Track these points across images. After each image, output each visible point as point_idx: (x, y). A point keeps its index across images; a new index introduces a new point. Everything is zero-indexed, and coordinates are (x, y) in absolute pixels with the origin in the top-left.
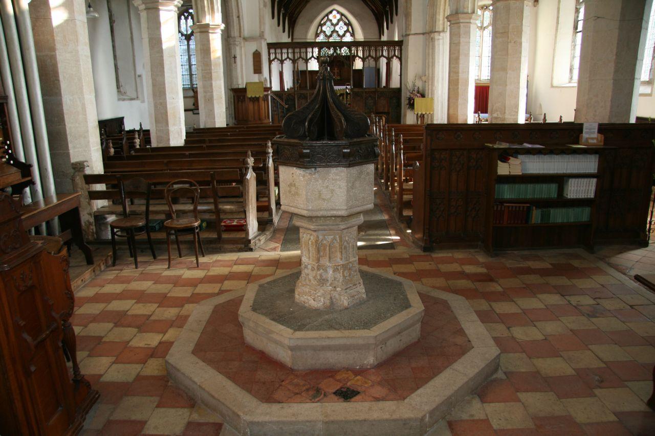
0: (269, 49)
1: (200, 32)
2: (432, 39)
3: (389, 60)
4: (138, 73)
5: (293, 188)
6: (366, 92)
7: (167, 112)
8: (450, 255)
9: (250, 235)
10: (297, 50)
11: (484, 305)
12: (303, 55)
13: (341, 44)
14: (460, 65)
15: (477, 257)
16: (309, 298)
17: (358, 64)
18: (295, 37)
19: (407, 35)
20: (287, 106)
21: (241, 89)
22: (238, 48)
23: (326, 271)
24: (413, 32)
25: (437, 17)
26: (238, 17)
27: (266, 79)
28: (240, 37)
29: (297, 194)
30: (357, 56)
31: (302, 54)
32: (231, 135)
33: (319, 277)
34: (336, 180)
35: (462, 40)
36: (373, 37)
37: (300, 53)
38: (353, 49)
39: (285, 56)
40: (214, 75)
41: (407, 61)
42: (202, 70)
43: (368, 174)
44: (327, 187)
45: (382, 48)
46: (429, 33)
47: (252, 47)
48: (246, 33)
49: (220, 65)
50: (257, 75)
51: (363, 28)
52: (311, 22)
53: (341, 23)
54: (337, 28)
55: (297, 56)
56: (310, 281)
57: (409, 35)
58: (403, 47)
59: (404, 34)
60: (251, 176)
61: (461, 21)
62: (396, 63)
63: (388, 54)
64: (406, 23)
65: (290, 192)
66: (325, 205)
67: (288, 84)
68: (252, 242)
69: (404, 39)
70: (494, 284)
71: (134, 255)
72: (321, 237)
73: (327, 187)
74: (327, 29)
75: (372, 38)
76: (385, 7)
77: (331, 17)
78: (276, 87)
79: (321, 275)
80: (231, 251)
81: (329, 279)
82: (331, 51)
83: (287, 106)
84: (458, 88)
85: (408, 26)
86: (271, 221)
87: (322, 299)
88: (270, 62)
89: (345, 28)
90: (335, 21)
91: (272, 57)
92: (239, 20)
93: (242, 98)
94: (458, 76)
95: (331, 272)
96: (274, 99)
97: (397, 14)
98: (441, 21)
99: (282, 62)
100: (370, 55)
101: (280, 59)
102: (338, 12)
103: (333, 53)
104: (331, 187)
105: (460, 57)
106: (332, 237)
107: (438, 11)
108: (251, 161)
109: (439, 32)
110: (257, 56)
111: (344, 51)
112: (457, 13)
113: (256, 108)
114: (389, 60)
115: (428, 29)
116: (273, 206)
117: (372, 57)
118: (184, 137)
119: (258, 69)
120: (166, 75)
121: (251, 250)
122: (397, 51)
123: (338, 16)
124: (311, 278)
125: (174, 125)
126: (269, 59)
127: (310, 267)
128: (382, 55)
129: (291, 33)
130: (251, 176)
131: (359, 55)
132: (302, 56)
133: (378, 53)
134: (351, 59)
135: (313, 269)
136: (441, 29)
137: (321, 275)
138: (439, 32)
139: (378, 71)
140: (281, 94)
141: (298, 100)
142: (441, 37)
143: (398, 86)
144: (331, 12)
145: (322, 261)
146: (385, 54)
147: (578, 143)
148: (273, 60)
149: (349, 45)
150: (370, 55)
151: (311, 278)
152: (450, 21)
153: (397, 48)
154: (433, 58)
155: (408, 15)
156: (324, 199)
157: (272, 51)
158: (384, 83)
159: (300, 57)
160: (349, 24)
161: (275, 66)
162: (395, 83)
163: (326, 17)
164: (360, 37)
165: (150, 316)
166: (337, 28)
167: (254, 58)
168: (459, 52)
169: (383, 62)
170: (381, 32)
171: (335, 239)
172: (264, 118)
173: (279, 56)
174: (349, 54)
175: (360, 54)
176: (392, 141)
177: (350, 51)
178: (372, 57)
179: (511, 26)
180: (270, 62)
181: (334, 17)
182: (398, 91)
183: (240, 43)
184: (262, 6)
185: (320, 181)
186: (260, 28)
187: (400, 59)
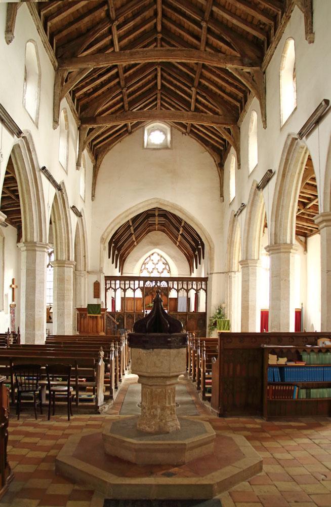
0: (106, 280)
1: (58, 266)
2: (230, 277)
3: (197, 291)
4: (5, 293)
5: (140, 360)
6: (179, 315)
7: (34, 321)
8: (237, 419)
9: (99, 403)
10: (127, 282)
11: (258, 443)
12: (113, 286)
13: (161, 279)
14: (250, 296)
15: (255, 420)
16: (146, 426)
17: (173, 294)
18: (124, 272)
19: (211, 274)
20: (118, 323)
21: (83, 308)
22: (83, 279)
23: (156, 409)
24: (215, 272)
25: (233, 261)
26: (85, 256)
27: (102, 302)
28: (85, 270)
29: (142, 364)
30: (173, 288)
31: (131, 285)
32: (79, 340)
33: (152, 414)
34: (165, 356)
35: (250, 278)
36: (185, 274)
37: (130, 284)
38: (171, 283)
39: (190, 287)
40: (66, 297)
41: (211, 293)
42: (57, 293)
43: (182, 354)
44: (159, 360)
45: (192, 283)
46: (227, 273)
47: (94, 278)
48: (89, 268)
49: (71, 290)
50: (96, 299)
51: (178, 267)
52: (137, 261)
53: (161, 263)
54: (157, 266)
55: (199, 287)
56: (146, 416)
57: (212, 274)
58: (208, 282)
59: (209, 272)
60: (101, 363)
61: (250, 265)
62: (202, 294)
63: (197, 288)
64: (210, 265)
65: (137, 363)
66: (158, 370)
67: (118, 308)
68: (100, 408)
69: (209, 276)
70: (265, 433)
71: (18, 413)
72: (154, 390)
73: (159, 360)
74: (150, 266)
75: (183, 274)
76: (194, 252)
77: (152, 257)
78: (110, 309)
79: (153, 412)
80: (85, 413)
81: (158, 415)
82: (154, 283)
83: (118, 323)
84: (248, 313)
85: (212, 267)
86: (112, 397)
87: (154, 427)
88: (106, 290)
89: (164, 266)
90: (155, 262)
91: (108, 286)
92: (85, 258)
93: (84, 315)
94: (248, 304)
95: (159, 410)
96: (108, 317)
97: (203, 258)
98: (236, 266)
99: (115, 290)
100: (183, 288)
101: (186, 288)
102: (158, 255)
103: (155, 286)
104: (162, 360)
105: (250, 290)
106: (160, 390)
107: (234, 256)
108: (102, 353)
109: (235, 272)
110: (97, 285)
111: (164, 284)
112: (247, 259)
113: (95, 323)
114: (197, 291)
115: (226, 270)
116: (113, 388)
117: (184, 289)
118: (45, 340)
119: (97, 295)
120: (36, 295)
121: (99, 413)
122: (203, 285)
123: (159, 258)
124: (148, 415)
125: (39, 330)
126: (106, 288)
127: (146, 408)
128: (192, 288)
129: (121, 270)
130: (101, 363)
131: (174, 287)
132: (131, 287)
133: (189, 286)
134: (168, 290)
135: (149, 409)
136: (236, 270)
137: (153, 412)
138: (235, 272)
139: (189, 300)
140: (114, 313)
141: (126, 319)
142: (236, 276)
143: (205, 311)
144: (153, 254)
145: (155, 404)
146: (195, 287)
147: (317, 345)
148: (109, 288)
149: (167, 280)
150: (183, 288)
151: (148, 415)
152: (241, 265)
153: (203, 283)
154: (231, 291)
155: (211, 259)
156: (157, 367)
157: (108, 282)
158: (192, 309)
159: (111, 287)
160: (166, 264)
161: (111, 293)
162: (202, 309)
163: (149, 258)
164: (175, 273)
165: (36, 443)
166: (157, 266)
167: (94, 287)
168: (249, 286)
169: (192, 294)
170: (191, 270)
171: (162, 391)
172: (100, 331)
173: (132, 286)
174: (167, 286)
175: (175, 286)
176: (198, 347)
177: (168, 284)
178: (184, 289)
179: (282, 270)
180: (106, 290)
181: (155, 258)
182: (204, 315)
183: (85, 275)
184: (102, 249)
185: (155, 357)
186: (100, 265)
187: (206, 291)
